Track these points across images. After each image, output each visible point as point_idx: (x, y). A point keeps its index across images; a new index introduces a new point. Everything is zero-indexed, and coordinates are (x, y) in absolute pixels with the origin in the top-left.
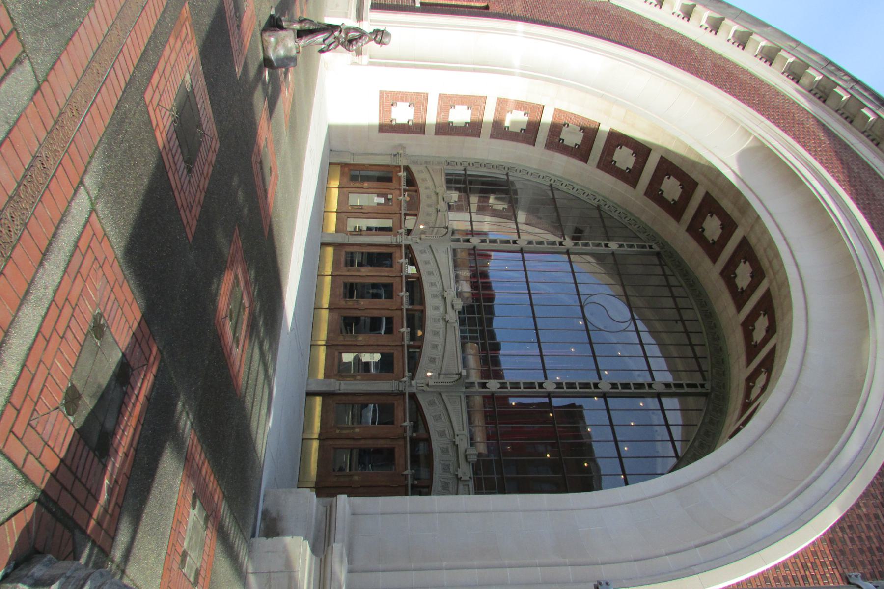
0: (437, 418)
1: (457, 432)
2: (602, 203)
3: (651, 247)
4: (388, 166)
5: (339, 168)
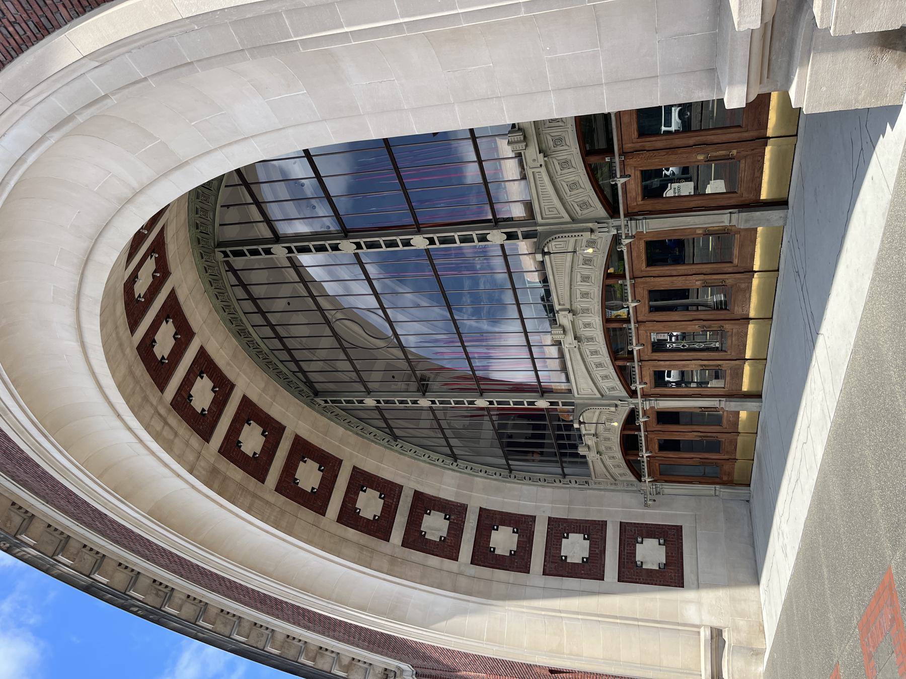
0: (573, 186)
1: (543, 170)
2: (393, 443)
3: (326, 402)
4: (666, 481)
5: (736, 477)
